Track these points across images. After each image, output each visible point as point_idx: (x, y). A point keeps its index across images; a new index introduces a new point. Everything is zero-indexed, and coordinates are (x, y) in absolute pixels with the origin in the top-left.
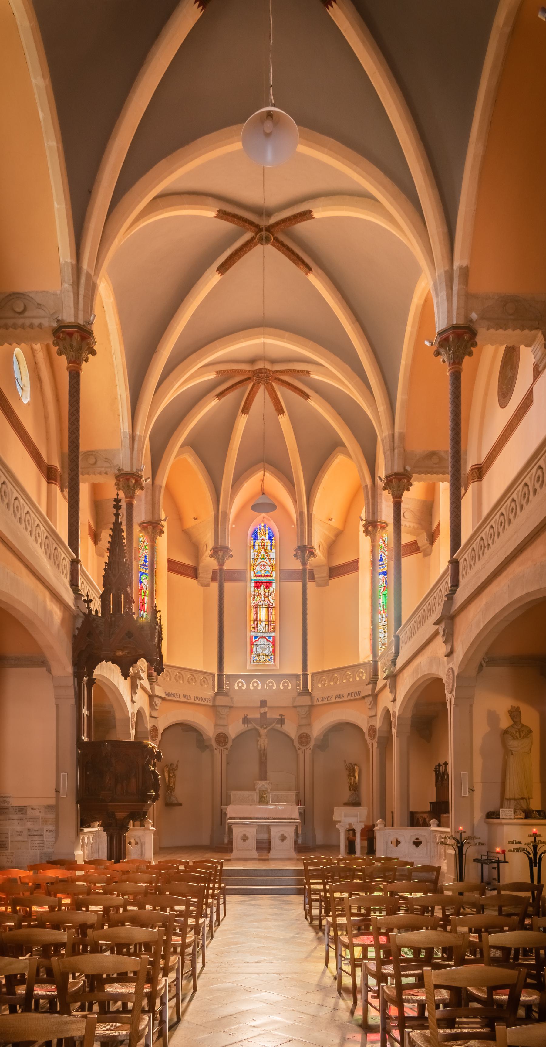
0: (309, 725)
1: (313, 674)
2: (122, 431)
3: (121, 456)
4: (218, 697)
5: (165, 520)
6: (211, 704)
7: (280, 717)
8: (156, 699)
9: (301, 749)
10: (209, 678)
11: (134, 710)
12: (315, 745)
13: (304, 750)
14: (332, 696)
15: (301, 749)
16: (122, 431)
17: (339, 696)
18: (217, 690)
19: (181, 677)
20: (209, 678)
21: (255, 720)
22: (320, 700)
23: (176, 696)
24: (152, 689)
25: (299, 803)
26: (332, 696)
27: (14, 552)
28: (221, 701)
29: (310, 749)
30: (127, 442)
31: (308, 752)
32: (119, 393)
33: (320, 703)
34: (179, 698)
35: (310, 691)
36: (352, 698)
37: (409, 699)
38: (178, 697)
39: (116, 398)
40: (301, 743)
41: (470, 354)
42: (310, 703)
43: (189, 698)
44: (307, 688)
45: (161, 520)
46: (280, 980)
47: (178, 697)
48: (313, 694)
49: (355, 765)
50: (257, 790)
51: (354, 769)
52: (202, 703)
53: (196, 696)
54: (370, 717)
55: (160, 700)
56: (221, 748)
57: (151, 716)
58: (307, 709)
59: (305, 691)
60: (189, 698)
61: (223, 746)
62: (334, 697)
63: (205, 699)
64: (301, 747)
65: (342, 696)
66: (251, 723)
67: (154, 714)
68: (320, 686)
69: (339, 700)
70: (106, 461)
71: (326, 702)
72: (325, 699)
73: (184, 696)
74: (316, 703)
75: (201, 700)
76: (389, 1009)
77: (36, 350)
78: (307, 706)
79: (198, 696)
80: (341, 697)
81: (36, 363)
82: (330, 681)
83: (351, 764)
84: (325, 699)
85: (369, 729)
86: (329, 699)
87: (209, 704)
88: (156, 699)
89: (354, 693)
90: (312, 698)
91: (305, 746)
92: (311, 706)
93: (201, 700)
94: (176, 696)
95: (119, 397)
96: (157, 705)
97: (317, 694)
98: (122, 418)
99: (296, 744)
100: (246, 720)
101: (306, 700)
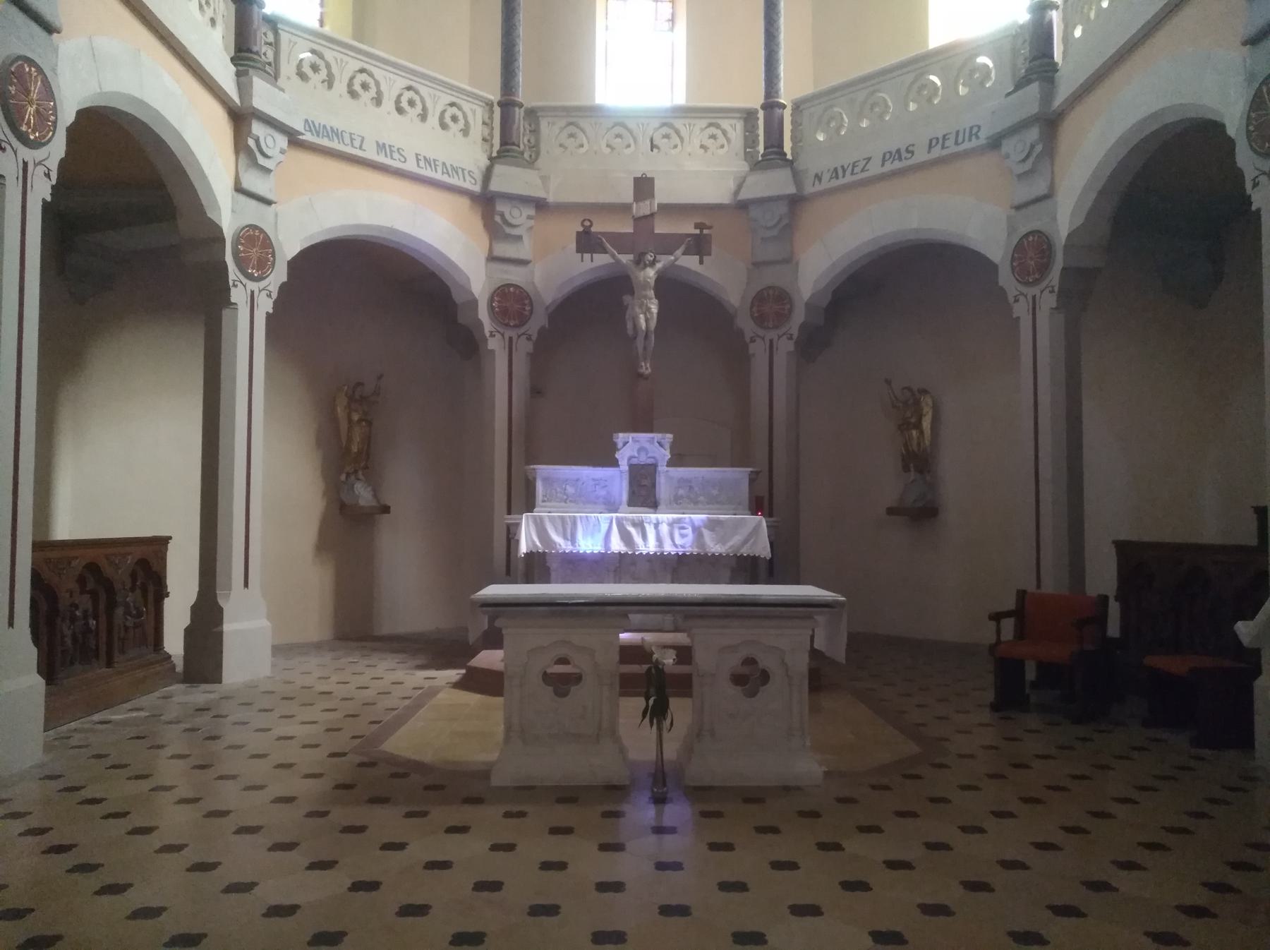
0: (789, 260)
1: (798, 107)
4: (499, 169)
6: (477, 188)
7: (698, 231)
8: (257, 128)
9: (758, 340)
10: (474, 112)
12: (803, 327)
13: (771, 341)
14: (869, 159)
15: (758, 340)
18: (498, 152)
19: (372, 84)
20: (474, 112)
21: (617, 239)
22: (826, 177)
23: (347, 140)
25: (757, 506)
26: (869, 159)
27: (320, 150)
28: (509, 179)
29: (790, 338)
31: (785, 347)
33: (826, 184)
34: (361, 148)
35: (789, 157)
36: (945, 152)
38: (357, 144)
40: (760, 320)
42: (791, 190)
43: (396, 155)
44: (781, 146)
46: (607, 29)
47: (357, 144)
48: (800, 165)
49: (924, 392)
50: (624, 466)
51: (917, 403)
52: (445, 178)
53: (423, 154)
54: (1018, 208)
55: (282, 141)
56: (509, 333)
57: (239, 189)
58: (783, 209)
59: (774, 155)
60: (396, 155)
61: (516, 326)
62: (877, 161)
63: (455, 170)
64: (761, 332)
65: (907, 151)
66: (605, 251)
67: (253, 181)
68: (821, 137)
69: (897, 165)
71: (849, 178)
72: (844, 171)
73: (381, 147)
74: (809, 189)
75: (440, 169)
78: (779, 198)
79: (431, 156)
80: (904, 155)
82: (860, 116)
83: (909, 389)
84: (844, 171)
85: (1020, 249)
86: (856, 170)
87: (468, 185)
89: (952, 138)
90: (797, 176)
91: (776, 327)
92: (795, 202)
93: (440, 169)
94: (347, 140)
96: (269, 152)
97: (812, 164)
99: (746, 324)
100: (587, 242)
101: (776, 183)
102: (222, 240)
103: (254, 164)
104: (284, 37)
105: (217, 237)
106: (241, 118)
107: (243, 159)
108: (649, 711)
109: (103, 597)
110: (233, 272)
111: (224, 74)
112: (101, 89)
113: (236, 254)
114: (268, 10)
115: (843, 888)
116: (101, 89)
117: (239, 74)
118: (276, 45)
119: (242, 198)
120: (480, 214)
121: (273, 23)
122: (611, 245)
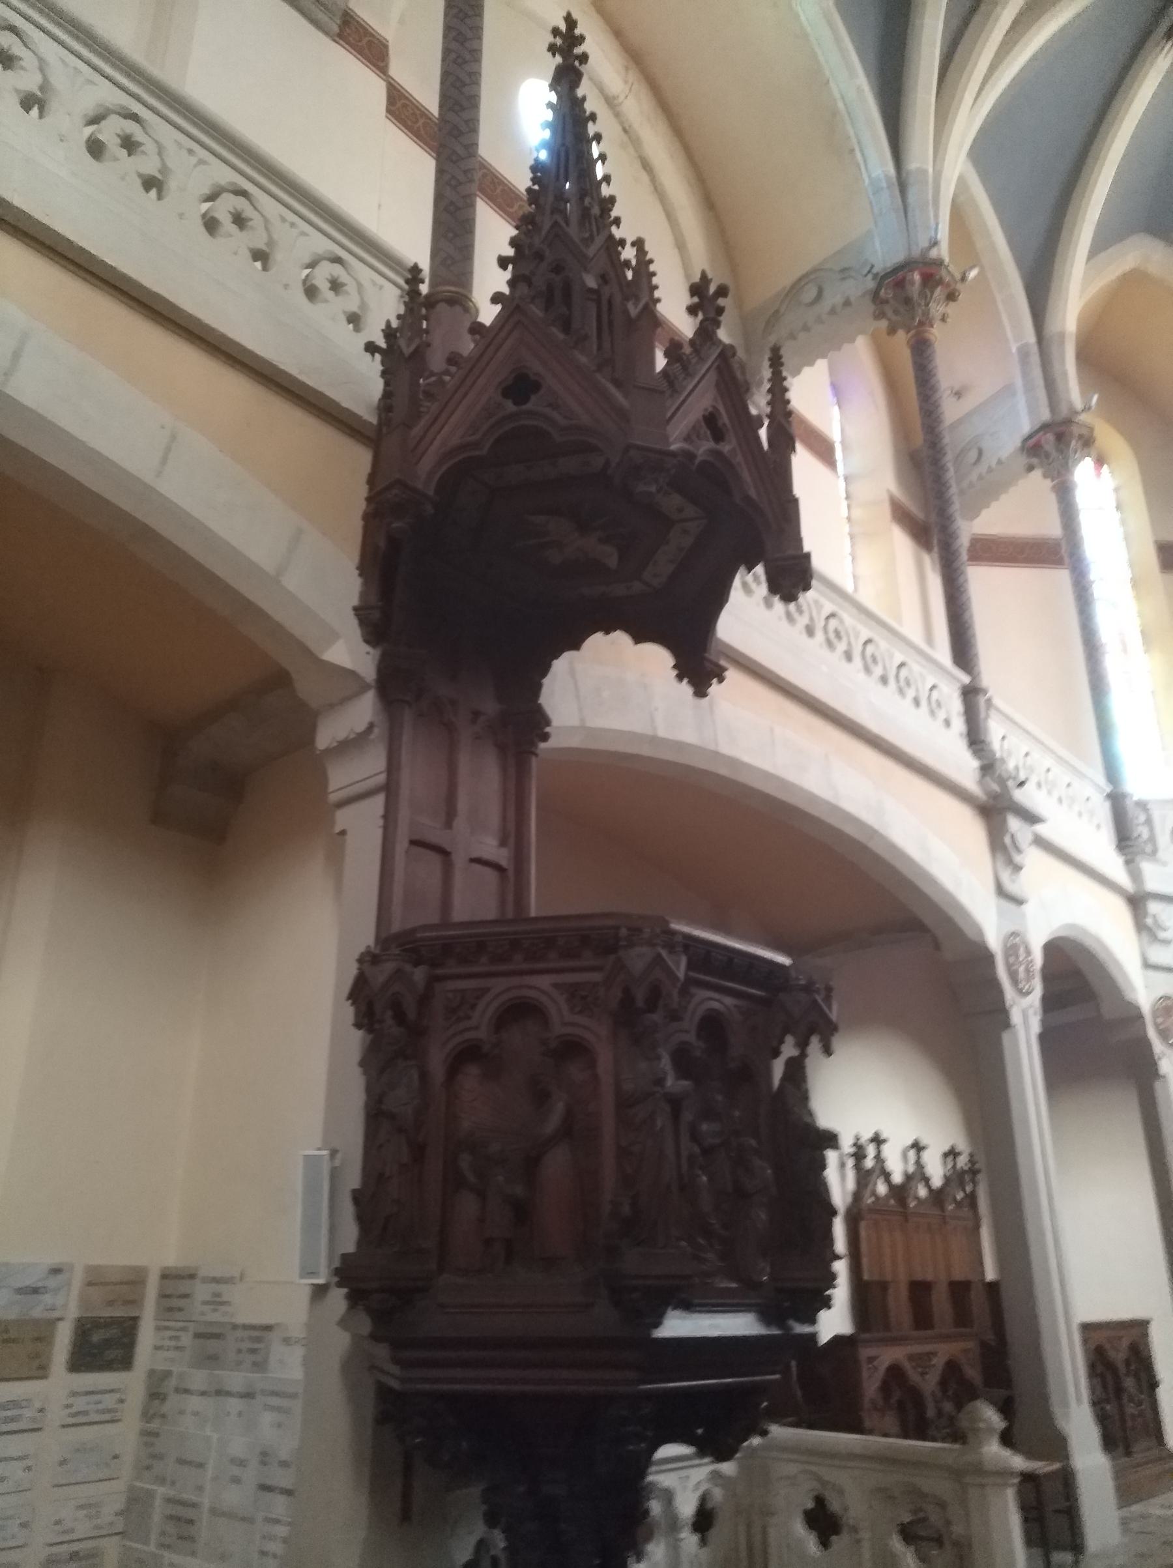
2: (867, 181)
3: (877, 244)
5: (1087, 409)
11: (1004, 1473)
16: (867, 181)
17: (191, 152)
24: (1136, 875)
30: (888, 199)
32: (837, 95)
37: (77, 275)
39: (835, 113)
41: (345, 1257)
45: (1077, 413)
57: (1147, 965)
70: (843, 279)
76: (1080, 420)
77: (614, 98)
81: (625, 131)
88: (1153, 907)
95: (841, 105)
98: (863, 155)
102: (1140, 1017)
103: (1154, 938)
104: (1156, 815)
105: (1136, 1016)
106: (1137, 902)
107: (1145, 937)
108: (931, 202)
109: (1109, 1377)
110: (1158, 1046)
111: (1113, 865)
112: (381, 773)
113: (1157, 1025)
114: (1135, 798)
115: (596, 119)
116: (381, 773)
117: (1128, 862)
118: (1149, 822)
119: (1152, 974)
120: (695, 330)
121: (1143, 805)
122: (650, 1384)
